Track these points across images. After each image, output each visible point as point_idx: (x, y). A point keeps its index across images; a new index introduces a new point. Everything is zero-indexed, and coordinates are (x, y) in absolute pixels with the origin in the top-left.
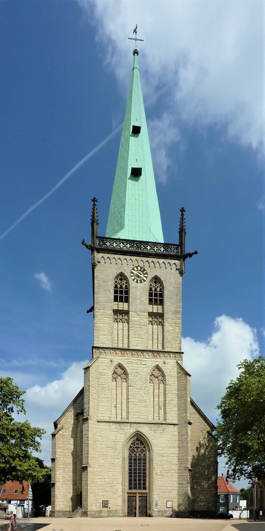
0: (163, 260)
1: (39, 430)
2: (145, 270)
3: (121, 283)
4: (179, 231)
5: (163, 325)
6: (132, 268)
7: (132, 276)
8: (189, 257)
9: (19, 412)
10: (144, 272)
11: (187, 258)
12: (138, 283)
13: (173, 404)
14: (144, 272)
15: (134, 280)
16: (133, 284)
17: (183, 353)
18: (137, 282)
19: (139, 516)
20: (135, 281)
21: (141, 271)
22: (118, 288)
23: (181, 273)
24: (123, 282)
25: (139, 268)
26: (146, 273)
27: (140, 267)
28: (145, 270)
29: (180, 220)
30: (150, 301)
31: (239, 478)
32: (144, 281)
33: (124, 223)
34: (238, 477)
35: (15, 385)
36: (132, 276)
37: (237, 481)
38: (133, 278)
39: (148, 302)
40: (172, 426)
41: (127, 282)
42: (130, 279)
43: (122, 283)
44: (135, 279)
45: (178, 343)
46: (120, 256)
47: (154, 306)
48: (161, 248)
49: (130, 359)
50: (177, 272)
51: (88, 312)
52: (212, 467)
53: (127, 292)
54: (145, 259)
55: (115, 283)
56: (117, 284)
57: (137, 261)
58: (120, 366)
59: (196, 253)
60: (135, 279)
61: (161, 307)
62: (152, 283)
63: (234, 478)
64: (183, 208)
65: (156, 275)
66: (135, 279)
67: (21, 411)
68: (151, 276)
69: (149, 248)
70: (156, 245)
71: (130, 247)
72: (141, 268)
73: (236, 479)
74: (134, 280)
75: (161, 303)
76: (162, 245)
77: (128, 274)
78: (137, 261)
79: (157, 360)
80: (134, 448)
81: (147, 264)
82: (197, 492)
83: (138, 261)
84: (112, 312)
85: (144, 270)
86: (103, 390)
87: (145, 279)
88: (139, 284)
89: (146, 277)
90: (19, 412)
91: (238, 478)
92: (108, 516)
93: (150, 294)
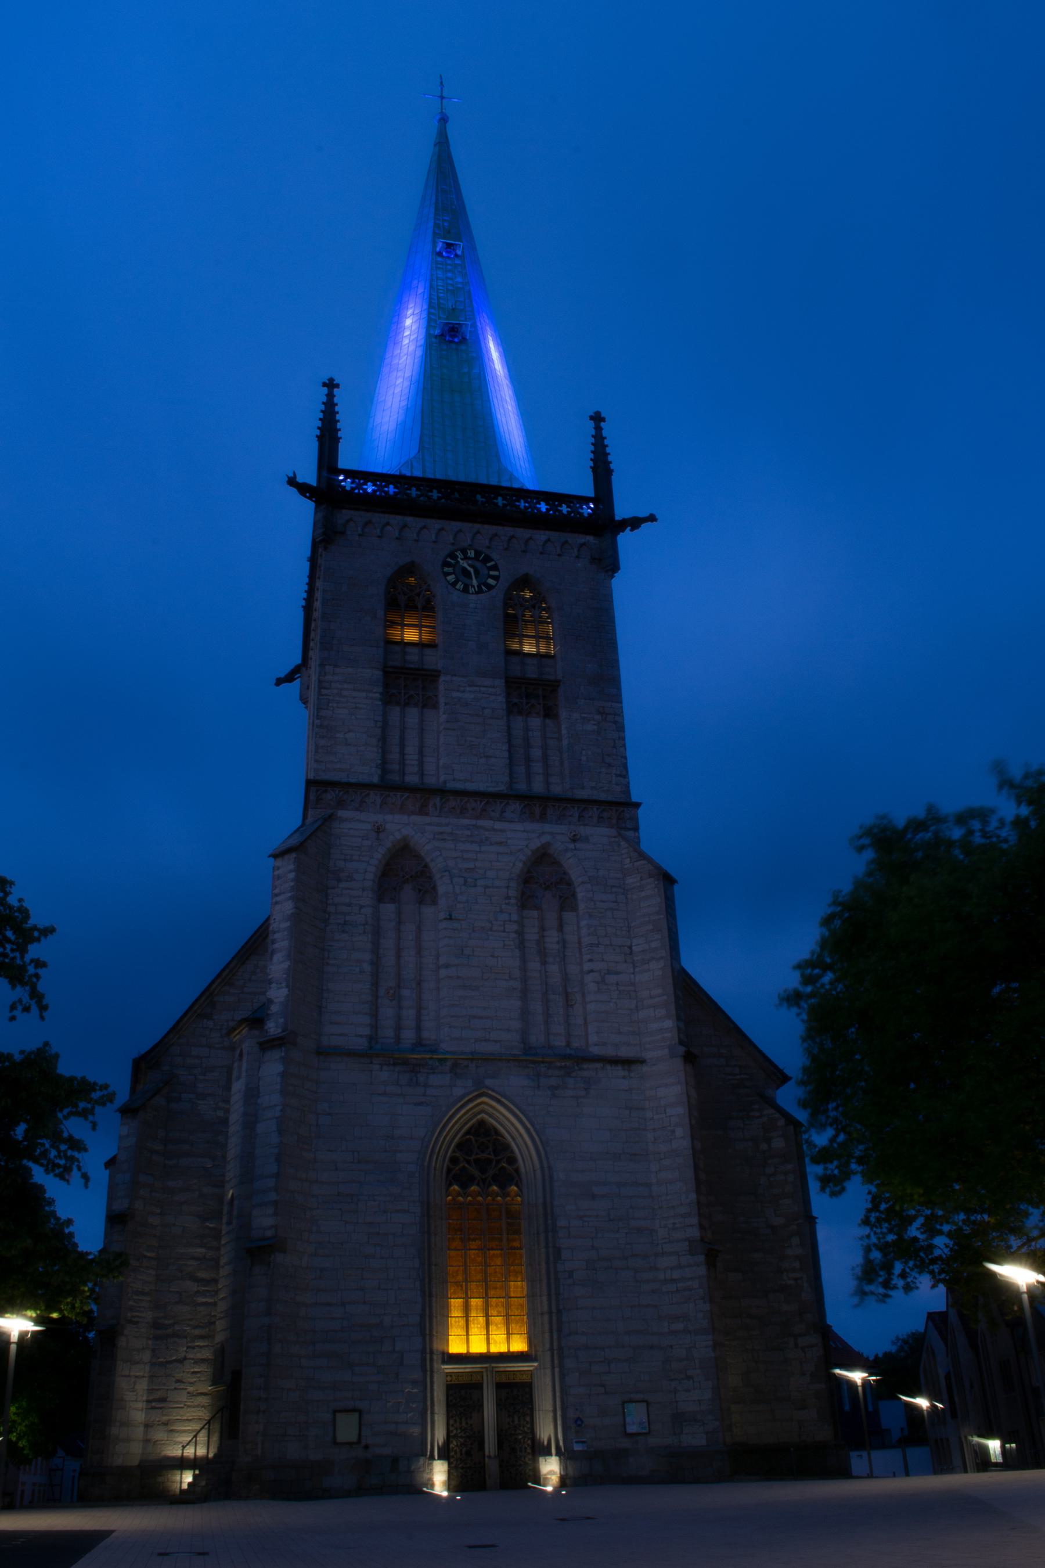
0: (547, 532)
1: (92, 1087)
4: (592, 465)
8: (632, 530)
9: (15, 1013)
11: (623, 531)
12: (468, 593)
13: (617, 984)
17: (637, 805)
18: (465, 590)
20: (458, 587)
21: (479, 560)
25: (471, 554)
26: (495, 568)
31: (909, 1280)
32: (490, 587)
33: (316, 513)
34: (903, 1275)
35: (16, 904)
36: (449, 574)
37: (898, 1295)
40: (620, 1067)
44: (460, 583)
45: (618, 773)
49: (447, 825)
51: (279, 682)
52: (795, 1240)
58: (404, 850)
59: (652, 518)
63: (886, 1284)
65: (527, 574)
67: (26, 1009)
69: (500, 501)
71: (439, 498)
73: (895, 1287)
79: (547, 828)
80: (468, 1162)
82: (81, 1330)
84: (381, 673)
86: (344, 932)
88: (473, 597)
90: (17, 1013)
91: (900, 1283)
92: (360, 1491)
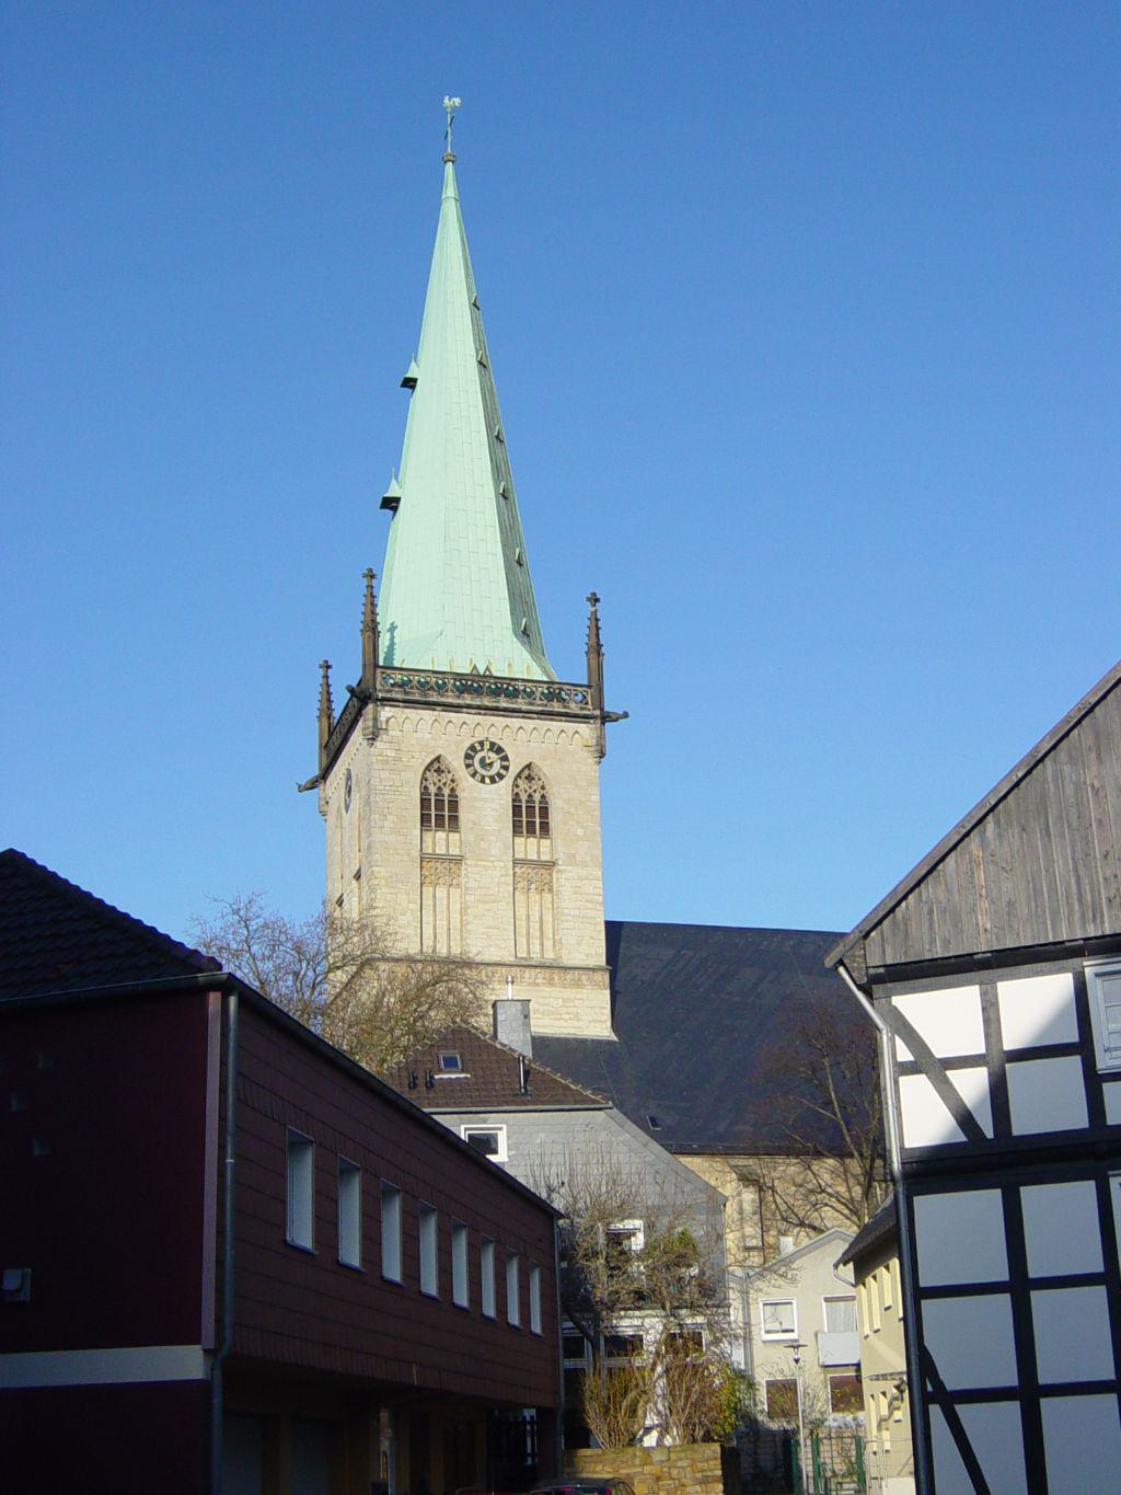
53: (454, 805)
64: (594, 594)
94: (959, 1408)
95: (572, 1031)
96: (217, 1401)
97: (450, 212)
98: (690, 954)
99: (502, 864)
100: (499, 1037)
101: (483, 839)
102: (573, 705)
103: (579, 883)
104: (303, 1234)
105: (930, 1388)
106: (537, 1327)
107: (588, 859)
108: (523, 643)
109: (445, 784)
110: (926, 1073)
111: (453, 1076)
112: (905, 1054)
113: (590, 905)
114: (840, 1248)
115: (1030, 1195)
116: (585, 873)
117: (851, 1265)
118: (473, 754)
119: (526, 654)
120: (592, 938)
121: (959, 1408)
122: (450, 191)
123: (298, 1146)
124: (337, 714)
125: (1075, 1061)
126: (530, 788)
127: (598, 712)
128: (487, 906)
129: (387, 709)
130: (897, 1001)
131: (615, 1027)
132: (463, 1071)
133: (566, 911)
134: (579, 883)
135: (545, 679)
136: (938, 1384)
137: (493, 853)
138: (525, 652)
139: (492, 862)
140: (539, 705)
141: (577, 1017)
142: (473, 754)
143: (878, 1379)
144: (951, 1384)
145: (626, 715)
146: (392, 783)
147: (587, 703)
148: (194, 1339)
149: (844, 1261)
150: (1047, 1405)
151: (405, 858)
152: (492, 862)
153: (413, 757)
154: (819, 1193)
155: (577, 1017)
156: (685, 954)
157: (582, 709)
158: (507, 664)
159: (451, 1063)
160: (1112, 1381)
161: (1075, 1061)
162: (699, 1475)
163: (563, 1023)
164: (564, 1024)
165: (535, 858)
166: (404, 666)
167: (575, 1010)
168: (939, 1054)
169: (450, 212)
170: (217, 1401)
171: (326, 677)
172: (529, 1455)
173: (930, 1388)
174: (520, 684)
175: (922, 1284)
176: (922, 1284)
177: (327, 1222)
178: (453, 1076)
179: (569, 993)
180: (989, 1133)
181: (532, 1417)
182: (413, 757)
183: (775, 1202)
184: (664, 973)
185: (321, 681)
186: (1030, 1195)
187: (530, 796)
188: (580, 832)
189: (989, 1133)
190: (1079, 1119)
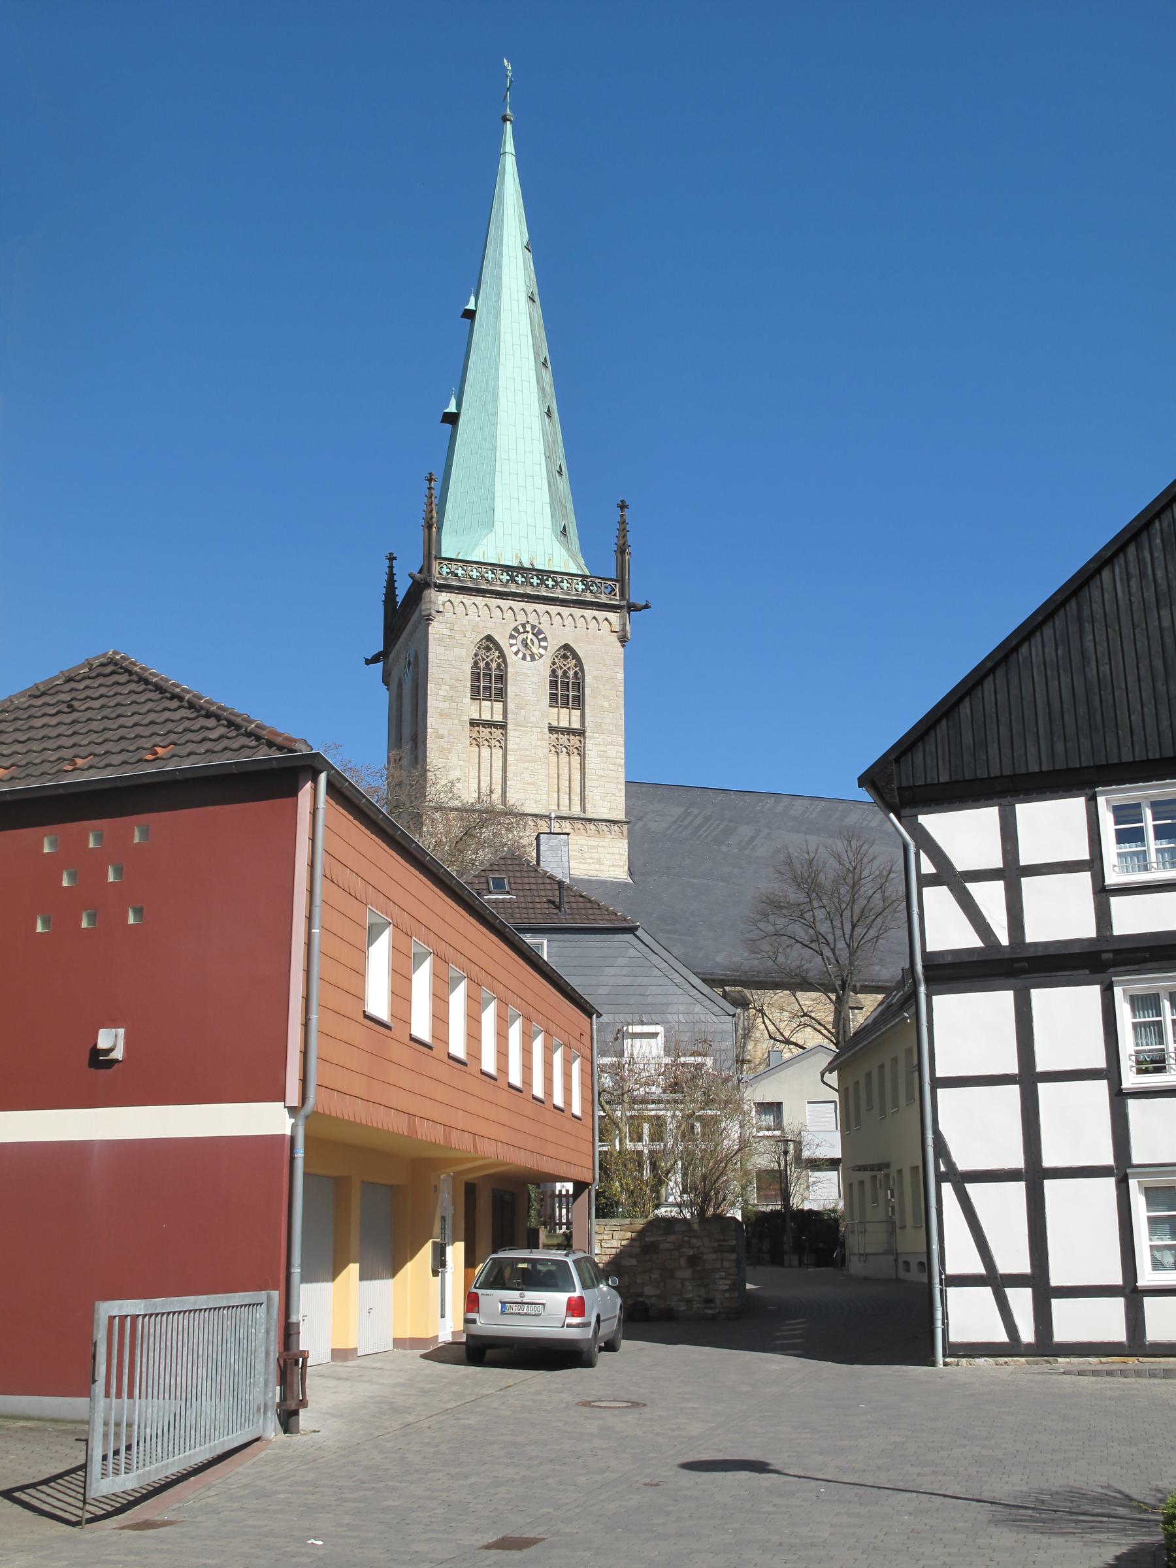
2: (542, 633)
3: (488, 657)
5: (582, 755)
6: (513, 628)
7: (511, 645)
10: (540, 637)
14: (540, 637)
15: (516, 653)
16: (516, 665)
18: (524, 658)
19: (1117, 831)
22: (480, 669)
23: (623, 640)
24: (492, 656)
26: (545, 639)
27: (530, 625)
28: (542, 633)
29: (618, 526)
30: (554, 701)
38: (515, 649)
39: (546, 699)
41: (502, 655)
42: (509, 652)
43: (490, 658)
44: (520, 652)
46: (596, 613)
47: (573, 711)
48: (458, 569)
50: (614, 638)
53: (502, 679)
54: (541, 608)
55: (551, 667)
56: (557, 668)
57: (476, 605)
60: (519, 651)
61: (578, 713)
62: (556, 660)
64: (622, 501)
66: (519, 651)
68: (554, 644)
70: (521, 572)
72: (533, 627)
74: (516, 653)
75: (579, 703)
76: (580, 579)
77: (503, 642)
78: (476, 605)
81: (545, 619)
83: (491, 608)
85: (540, 632)
87: (542, 651)
89: (545, 648)
93: (553, 684)
94: (969, 1187)
95: (595, 873)
96: (300, 1154)
97: (510, 164)
98: (696, 812)
99: (539, 730)
100: (541, 865)
101: (522, 708)
102: (603, 596)
103: (604, 748)
104: (378, 1004)
105: (943, 1168)
106: (576, 1110)
107: (612, 728)
108: (561, 543)
109: (492, 660)
110: (948, 885)
111: (501, 897)
112: (928, 867)
113: (612, 767)
114: (825, 1060)
115: (1039, 996)
116: (609, 739)
117: (835, 1073)
118: (516, 635)
119: (564, 552)
120: (614, 795)
121: (969, 1187)
122: (509, 146)
123: (373, 933)
124: (399, 599)
125: (1086, 877)
126: (565, 665)
127: (624, 603)
128: (526, 765)
129: (443, 594)
130: (922, 819)
131: (631, 873)
132: (508, 893)
133: (594, 771)
134: (604, 748)
135: (579, 573)
136: (950, 1164)
137: (531, 720)
138: (563, 550)
139: (531, 727)
140: (574, 595)
141: (599, 862)
142: (516, 635)
143: (859, 1170)
144: (962, 1166)
145: (647, 607)
146: (446, 658)
147: (615, 595)
148: (279, 1095)
149: (830, 1069)
150: (1051, 1187)
151: (456, 722)
152: (531, 727)
153: (465, 636)
154: (802, 1016)
155: (599, 862)
156: (692, 812)
157: (610, 599)
158: (547, 559)
159: (499, 885)
160: (1026, 1185)
161: (1086, 877)
162: (716, 1244)
163: (587, 867)
164: (589, 868)
165: (567, 725)
166: (460, 558)
167: (597, 856)
168: (959, 867)
169: (510, 164)
170: (300, 1154)
171: (391, 567)
172: (564, 1224)
173: (943, 1168)
174: (558, 576)
175: (939, 1074)
176: (939, 1074)
177: (401, 995)
178: (501, 897)
179: (593, 842)
180: (1004, 940)
181: (567, 1191)
182: (465, 636)
183: (764, 1022)
184: (673, 827)
185: (387, 570)
186: (1039, 996)
187: (565, 673)
188: (606, 704)
189: (1004, 940)
190: (1089, 930)
